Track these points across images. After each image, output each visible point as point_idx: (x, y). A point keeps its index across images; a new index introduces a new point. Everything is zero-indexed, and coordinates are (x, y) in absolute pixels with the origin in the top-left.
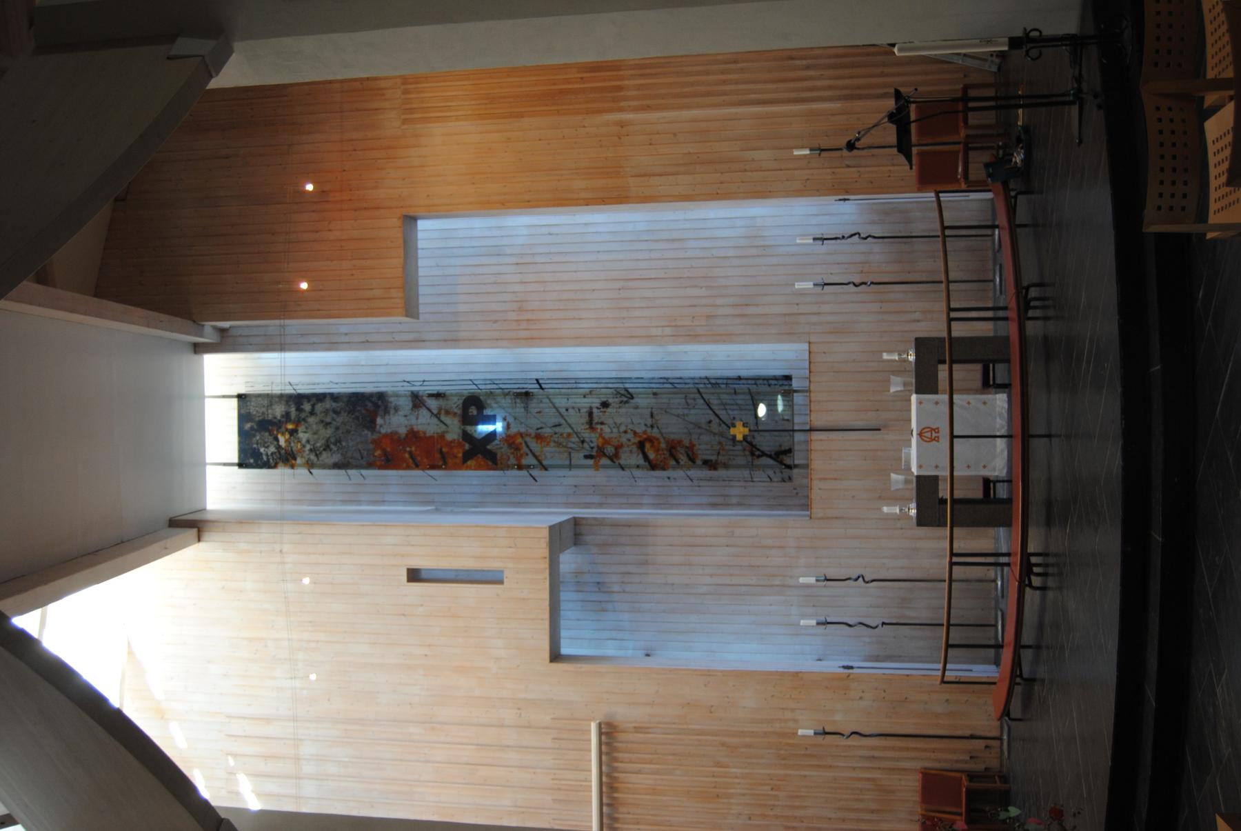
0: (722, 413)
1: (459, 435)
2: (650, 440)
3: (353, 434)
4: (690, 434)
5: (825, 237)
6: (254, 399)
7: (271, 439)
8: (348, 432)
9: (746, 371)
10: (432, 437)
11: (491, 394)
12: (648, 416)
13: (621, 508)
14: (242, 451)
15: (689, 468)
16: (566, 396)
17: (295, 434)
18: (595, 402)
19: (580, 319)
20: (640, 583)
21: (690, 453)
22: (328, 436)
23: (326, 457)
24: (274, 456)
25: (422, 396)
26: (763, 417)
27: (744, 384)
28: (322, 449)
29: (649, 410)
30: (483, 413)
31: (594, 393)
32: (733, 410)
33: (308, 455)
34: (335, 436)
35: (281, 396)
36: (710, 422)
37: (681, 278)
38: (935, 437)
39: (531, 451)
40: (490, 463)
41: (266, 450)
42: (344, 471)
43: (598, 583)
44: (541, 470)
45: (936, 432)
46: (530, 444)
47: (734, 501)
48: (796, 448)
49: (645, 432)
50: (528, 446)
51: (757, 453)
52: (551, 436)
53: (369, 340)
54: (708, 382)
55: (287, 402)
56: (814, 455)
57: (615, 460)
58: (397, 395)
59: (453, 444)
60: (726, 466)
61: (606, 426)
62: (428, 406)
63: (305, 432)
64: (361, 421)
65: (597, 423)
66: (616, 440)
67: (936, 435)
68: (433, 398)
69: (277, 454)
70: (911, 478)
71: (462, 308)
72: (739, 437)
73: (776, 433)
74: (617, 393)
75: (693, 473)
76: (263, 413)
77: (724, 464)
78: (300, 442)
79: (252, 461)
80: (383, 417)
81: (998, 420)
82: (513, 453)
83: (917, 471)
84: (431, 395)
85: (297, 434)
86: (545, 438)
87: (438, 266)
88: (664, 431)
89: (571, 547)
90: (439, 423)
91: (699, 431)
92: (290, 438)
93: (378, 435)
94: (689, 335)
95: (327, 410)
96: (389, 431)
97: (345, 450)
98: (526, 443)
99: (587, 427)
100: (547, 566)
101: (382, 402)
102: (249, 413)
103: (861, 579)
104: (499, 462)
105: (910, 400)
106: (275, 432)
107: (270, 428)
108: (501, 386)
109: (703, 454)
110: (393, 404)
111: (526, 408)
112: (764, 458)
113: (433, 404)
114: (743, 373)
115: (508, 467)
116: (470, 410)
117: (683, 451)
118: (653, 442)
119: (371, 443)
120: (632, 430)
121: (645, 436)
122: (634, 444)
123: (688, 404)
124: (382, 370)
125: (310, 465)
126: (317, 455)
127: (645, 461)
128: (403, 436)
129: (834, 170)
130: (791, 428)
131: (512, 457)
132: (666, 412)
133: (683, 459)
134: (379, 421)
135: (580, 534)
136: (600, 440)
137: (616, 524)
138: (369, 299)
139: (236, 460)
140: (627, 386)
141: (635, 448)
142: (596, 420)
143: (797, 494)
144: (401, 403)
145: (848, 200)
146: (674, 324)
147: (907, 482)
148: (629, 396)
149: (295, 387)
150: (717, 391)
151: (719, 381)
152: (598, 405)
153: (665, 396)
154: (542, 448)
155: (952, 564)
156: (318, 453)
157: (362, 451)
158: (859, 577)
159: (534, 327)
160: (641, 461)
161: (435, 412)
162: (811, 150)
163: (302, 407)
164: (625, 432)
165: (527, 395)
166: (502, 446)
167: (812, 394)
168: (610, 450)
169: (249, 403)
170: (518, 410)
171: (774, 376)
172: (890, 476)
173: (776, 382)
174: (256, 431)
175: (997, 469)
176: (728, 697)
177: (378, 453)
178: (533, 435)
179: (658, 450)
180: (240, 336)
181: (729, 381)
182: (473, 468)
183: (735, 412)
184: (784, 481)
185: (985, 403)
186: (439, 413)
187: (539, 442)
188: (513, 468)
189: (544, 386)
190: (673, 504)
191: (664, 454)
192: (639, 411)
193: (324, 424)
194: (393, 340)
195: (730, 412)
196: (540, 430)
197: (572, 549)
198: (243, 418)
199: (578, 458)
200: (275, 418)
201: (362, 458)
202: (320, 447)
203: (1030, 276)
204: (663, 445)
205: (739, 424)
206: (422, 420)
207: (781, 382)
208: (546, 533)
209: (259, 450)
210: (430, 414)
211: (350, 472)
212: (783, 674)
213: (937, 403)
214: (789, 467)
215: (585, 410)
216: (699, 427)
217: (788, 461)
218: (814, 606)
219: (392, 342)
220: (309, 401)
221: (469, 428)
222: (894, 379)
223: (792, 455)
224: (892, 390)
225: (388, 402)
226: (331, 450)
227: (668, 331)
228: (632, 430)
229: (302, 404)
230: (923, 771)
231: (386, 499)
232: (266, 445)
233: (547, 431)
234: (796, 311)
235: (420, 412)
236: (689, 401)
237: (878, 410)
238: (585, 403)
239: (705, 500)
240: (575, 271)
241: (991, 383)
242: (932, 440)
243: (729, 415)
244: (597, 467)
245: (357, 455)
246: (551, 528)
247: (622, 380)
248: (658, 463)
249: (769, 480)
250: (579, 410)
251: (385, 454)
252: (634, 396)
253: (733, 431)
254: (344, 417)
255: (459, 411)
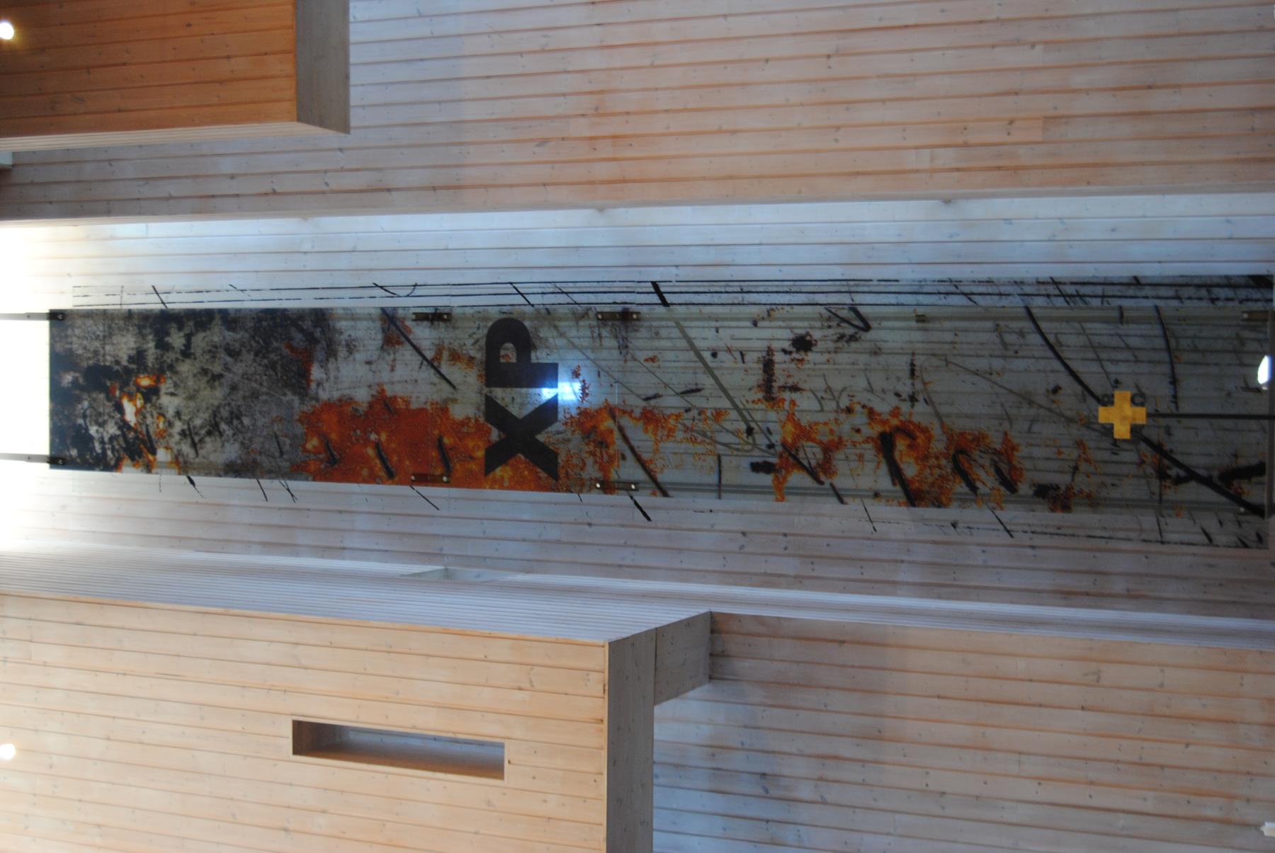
1: (478, 409)
2: (907, 430)
3: (265, 402)
4: (1009, 418)
6: (79, 322)
7: (108, 407)
8: (255, 395)
9: (1157, 265)
10: (421, 411)
11: (547, 315)
12: (905, 374)
13: (845, 590)
14: (58, 432)
15: (1000, 505)
16: (713, 324)
17: (154, 398)
18: (780, 336)
19: (734, 132)
20: (864, 783)
21: (1004, 467)
22: (216, 403)
23: (215, 451)
24: (115, 443)
25: (404, 319)
26: (1264, 385)
27: (1146, 297)
28: (203, 432)
29: (907, 359)
30: (529, 358)
31: (775, 314)
32: (1116, 362)
33: (178, 443)
34: (229, 404)
35: (129, 315)
36: (1056, 390)
39: (632, 449)
40: (543, 475)
41: (101, 430)
42: (254, 481)
43: (764, 775)
44: (654, 494)
46: (629, 433)
47: (1119, 586)
49: (895, 412)
50: (626, 439)
51: (1174, 472)
52: (678, 416)
53: (278, 190)
54: (1057, 292)
55: (140, 328)
57: (823, 478)
58: (352, 316)
59: (465, 430)
60: (1093, 502)
61: (806, 394)
62: (414, 342)
63: (172, 394)
64: (279, 375)
65: (783, 388)
66: (827, 429)
68: (425, 323)
69: (121, 440)
71: (471, 112)
72: (1122, 431)
73: (1228, 423)
74: (832, 316)
75: (1014, 515)
76: (96, 353)
77: (1089, 496)
78: (163, 415)
79: (74, 452)
80: (324, 365)
82: (593, 454)
84: (421, 317)
85: (158, 398)
86: (666, 419)
87: (421, 16)
88: (944, 410)
89: (700, 684)
90: (436, 379)
91: (1033, 411)
92: (144, 407)
93: (314, 402)
94: (999, 168)
95: (215, 347)
96: (336, 395)
97: (249, 435)
98: (621, 429)
99: (760, 395)
100: (604, 741)
101: (323, 332)
102: (71, 350)
104: (562, 473)
106: (117, 393)
107: (108, 383)
108: (577, 298)
109: (1036, 470)
110: (344, 337)
111: (624, 347)
112: (1193, 484)
113: (424, 335)
114: (1148, 271)
115: (580, 486)
116: (502, 353)
117: (986, 461)
118: (913, 438)
119: (300, 421)
120: (864, 407)
121: (895, 422)
122: (868, 439)
123: (1005, 345)
124: (342, 262)
125: (182, 465)
126: (194, 445)
127: (894, 484)
128: (363, 408)
131: (590, 461)
132: (947, 362)
133: (987, 481)
134: (316, 373)
135: (724, 655)
136: (790, 427)
137: (807, 636)
138: (221, 82)
139: (45, 450)
140: (859, 299)
141: (869, 451)
142: (780, 379)
144: (360, 334)
146: (960, 140)
148: (860, 324)
149: (163, 297)
152: (787, 345)
153: (947, 324)
154: (656, 442)
156: (197, 439)
157: (281, 439)
159: (630, 153)
160: (884, 482)
161: (429, 355)
163: (167, 339)
164: (849, 410)
165: (624, 318)
166: (569, 435)
168: (812, 453)
169: (69, 332)
170: (605, 354)
171: (1227, 277)
174: (83, 389)
177: (313, 443)
178: (637, 412)
179: (926, 457)
180: (32, 183)
181: (1110, 290)
182: (506, 484)
183: (1122, 368)
184: (1246, 546)
186: (438, 356)
187: (651, 428)
188: (591, 488)
189: (669, 298)
190: (968, 587)
191: (939, 467)
192: (882, 359)
193: (210, 375)
194: (325, 188)
196: (653, 402)
197: (704, 690)
198: (60, 361)
199: (738, 472)
200: (117, 363)
201: (282, 453)
202: (202, 427)
204: (938, 445)
205: (1122, 398)
206: (401, 372)
207: (1242, 293)
208: (601, 660)
209: (87, 429)
210: (421, 358)
211: (265, 482)
215: (755, 356)
216: (1031, 403)
219: (323, 193)
220: (180, 329)
221: (500, 394)
223: (1265, 479)
225: (335, 330)
226: (221, 434)
227: (947, 157)
228: (864, 407)
229: (168, 334)
231: (347, 544)
232: (101, 420)
233: (671, 403)
235: (398, 356)
236: (1010, 338)
238: (757, 339)
240: (725, 16)
243: (1107, 374)
244: (780, 492)
245: (273, 448)
246: (618, 649)
247: (850, 286)
248: (925, 487)
249: (1204, 539)
250: (742, 355)
251: (326, 445)
252: (873, 324)
253: (1104, 415)
254: (246, 365)
255: (479, 355)
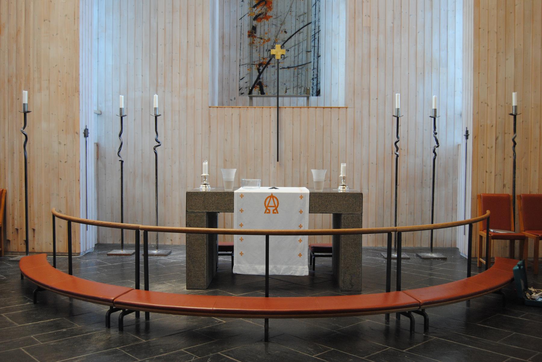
0: (291, 42)
5: (437, 119)
21: (261, 16)
36: (286, 32)
37: (401, 7)
38: (269, 210)
45: (274, 210)
47: (226, 53)
48: (265, 99)
51: (261, 68)
56: (258, 110)
60: (251, 44)
67: (271, 212)
70: (233, 186)
72: (273, 52)
75: (247, 20)
81: (284, 267)
83: (238, 193)
103: (158, 144)
105: (300, 186)
114: (322, 60)
117: (263, 11)
129: (494, 126)
130: (280, 94)
133: (257, 11)
143: (231, 100)
145: (467, 138)
147: (229, 183)
150: (309, 38)
151: (316, 41)
155: (137, 230)
158: (159, 142)
162: (516, 107)
167: (306, 109)
172: (234, 168)
173: (315, 84)
175: (240, 265)
176: (57, 34)
181: (316, 48)
183: (293, 52)
184: (240, 90)
185: (300, 255)
195: (293, 49)
203: (431, 313)
207: (315, 88)
212: (77, 79)
213: (301, 212)
214: (250, 92)
216: (281, 24)
217: (256, 92)
218: (142, 109)
222: (323, 173)
223: (260, 95)
224: (313, 171)
230: (4, 192)
234: (371, 98)
237: (293, 160)
239: (226, 30)
241: (316, 254)
242: (267, 207)
